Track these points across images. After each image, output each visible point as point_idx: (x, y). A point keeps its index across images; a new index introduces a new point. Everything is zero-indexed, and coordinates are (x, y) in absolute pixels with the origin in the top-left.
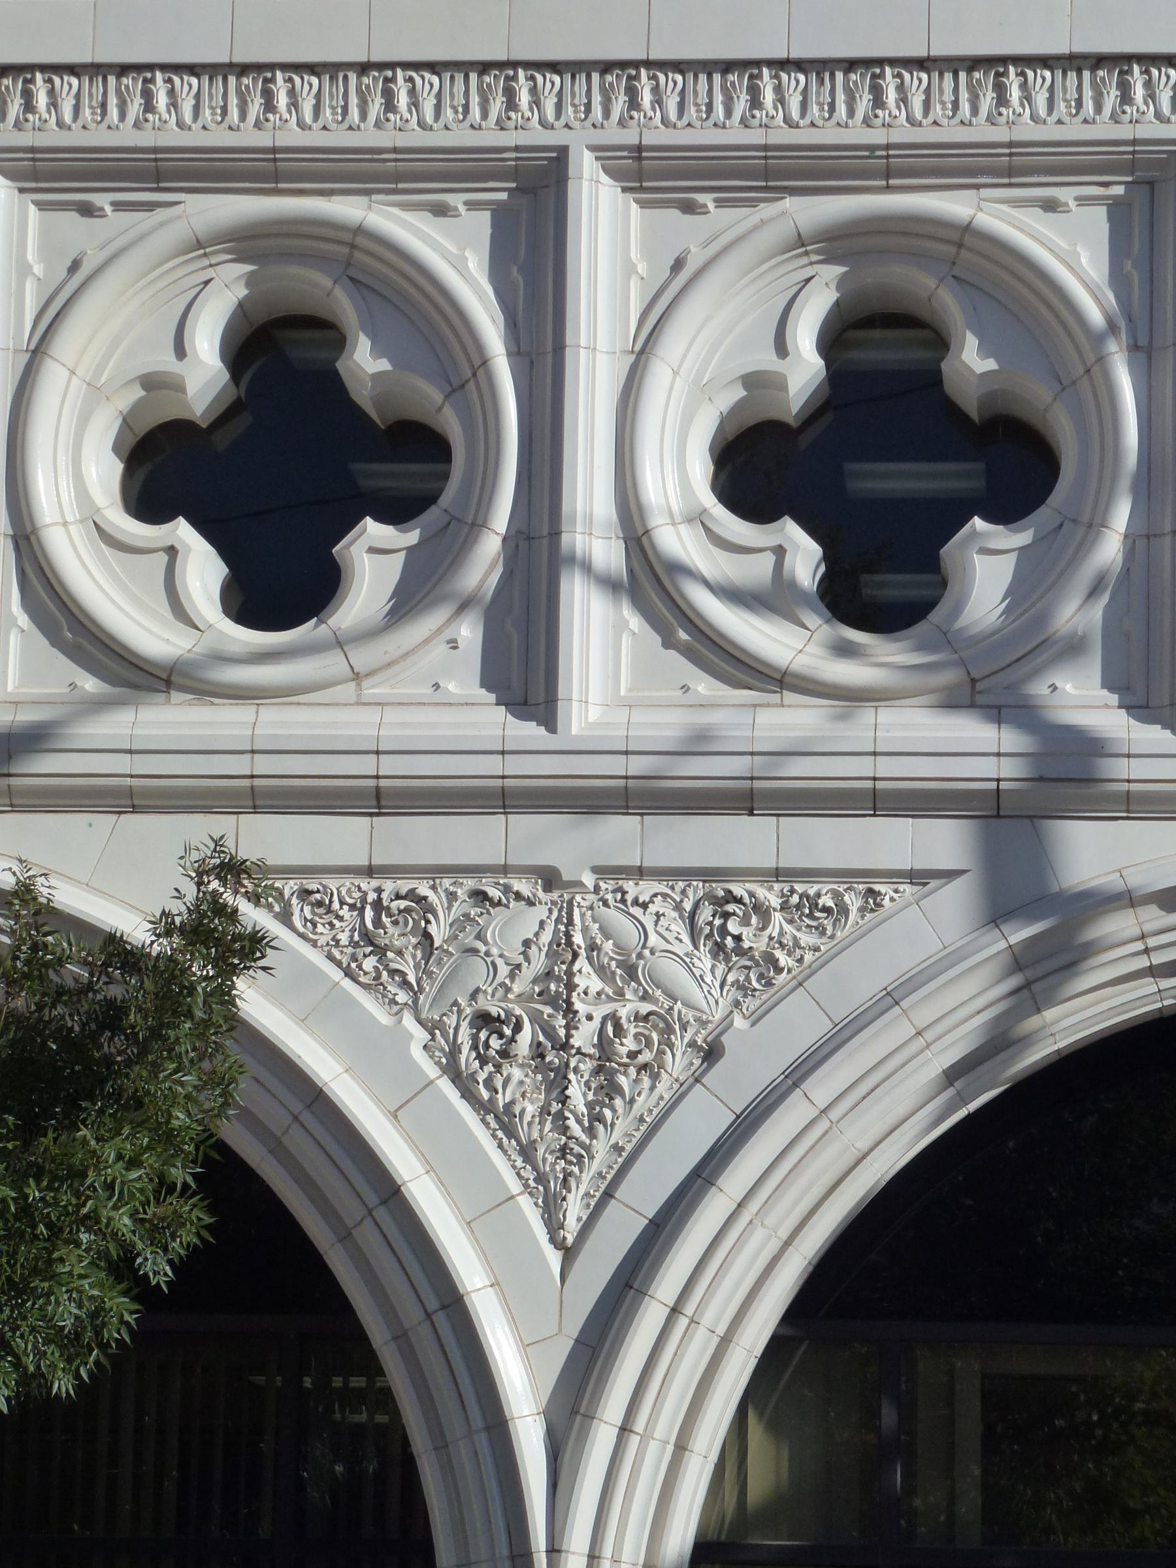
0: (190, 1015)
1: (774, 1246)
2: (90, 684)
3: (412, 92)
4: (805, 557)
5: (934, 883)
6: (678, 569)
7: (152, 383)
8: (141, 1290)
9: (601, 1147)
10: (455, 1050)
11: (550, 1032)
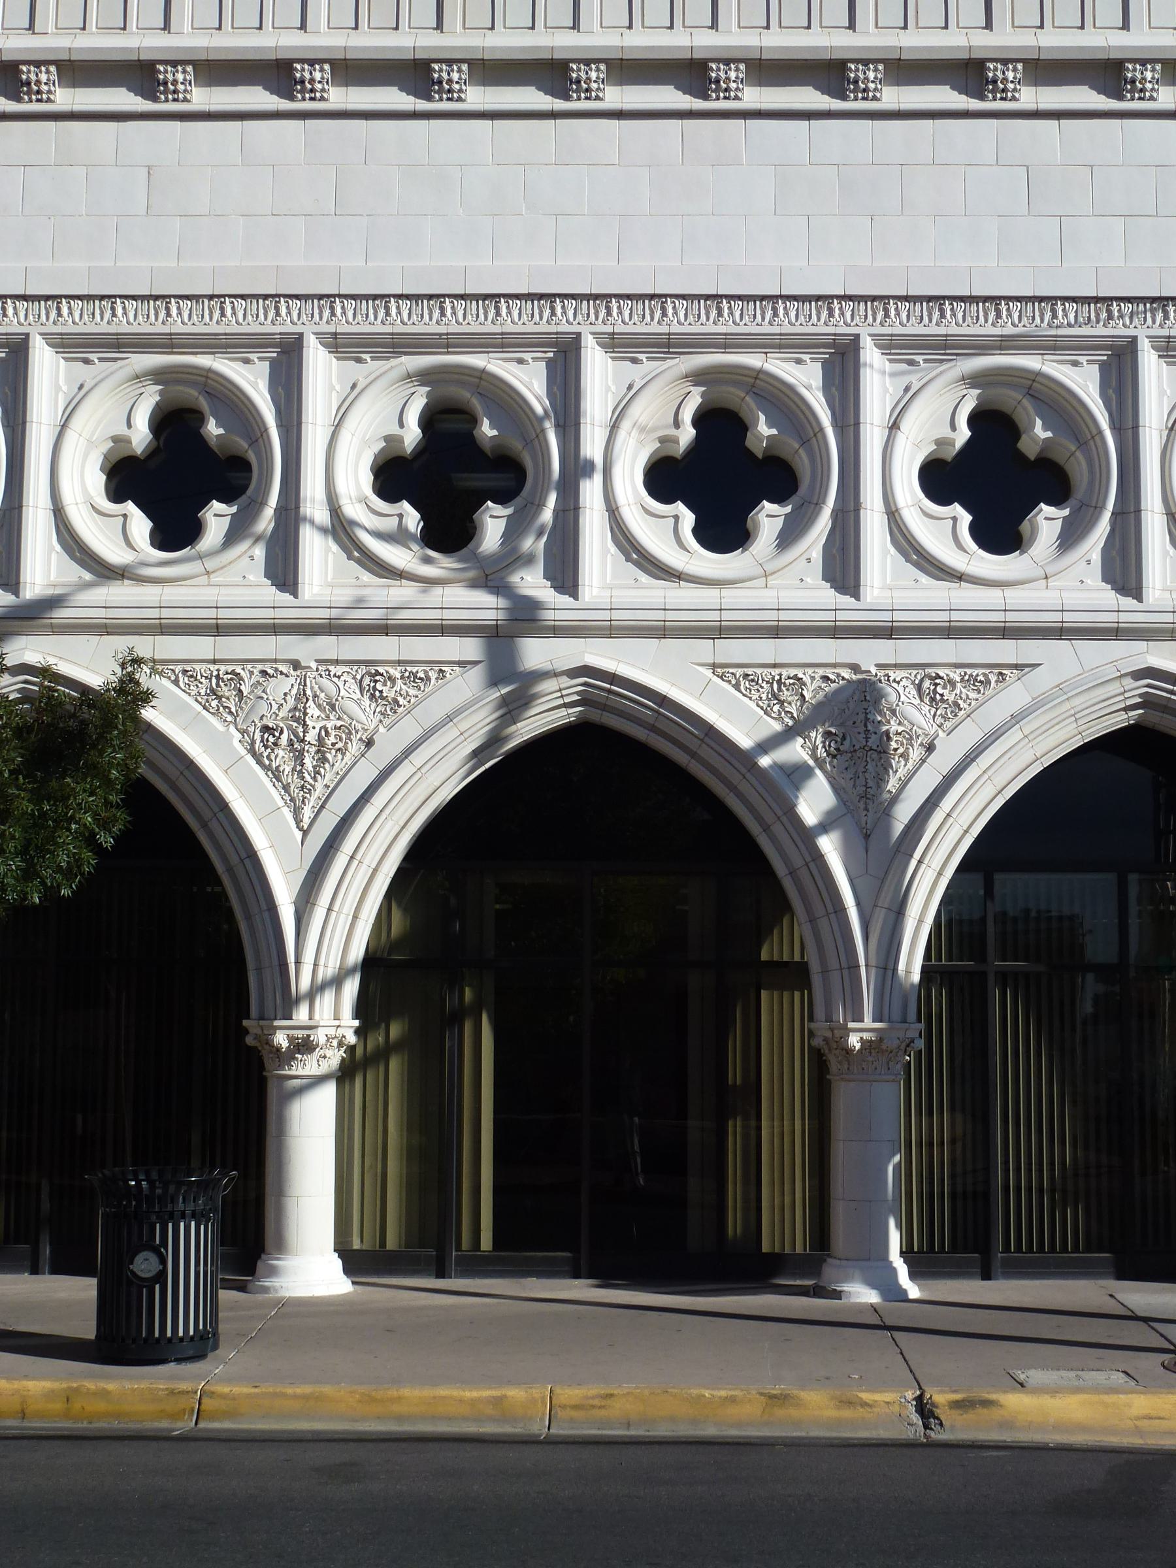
0: (116, 728)
1: (397, 829)
2: (88, 576)
3: (233, 308)
4: (413, 519)
5: (1027, 670)
6: (353, 523)
7: (116, 439)
8: (98, 850)
9: (319, 786)
10: (253, 742)
11: (296, 734)
